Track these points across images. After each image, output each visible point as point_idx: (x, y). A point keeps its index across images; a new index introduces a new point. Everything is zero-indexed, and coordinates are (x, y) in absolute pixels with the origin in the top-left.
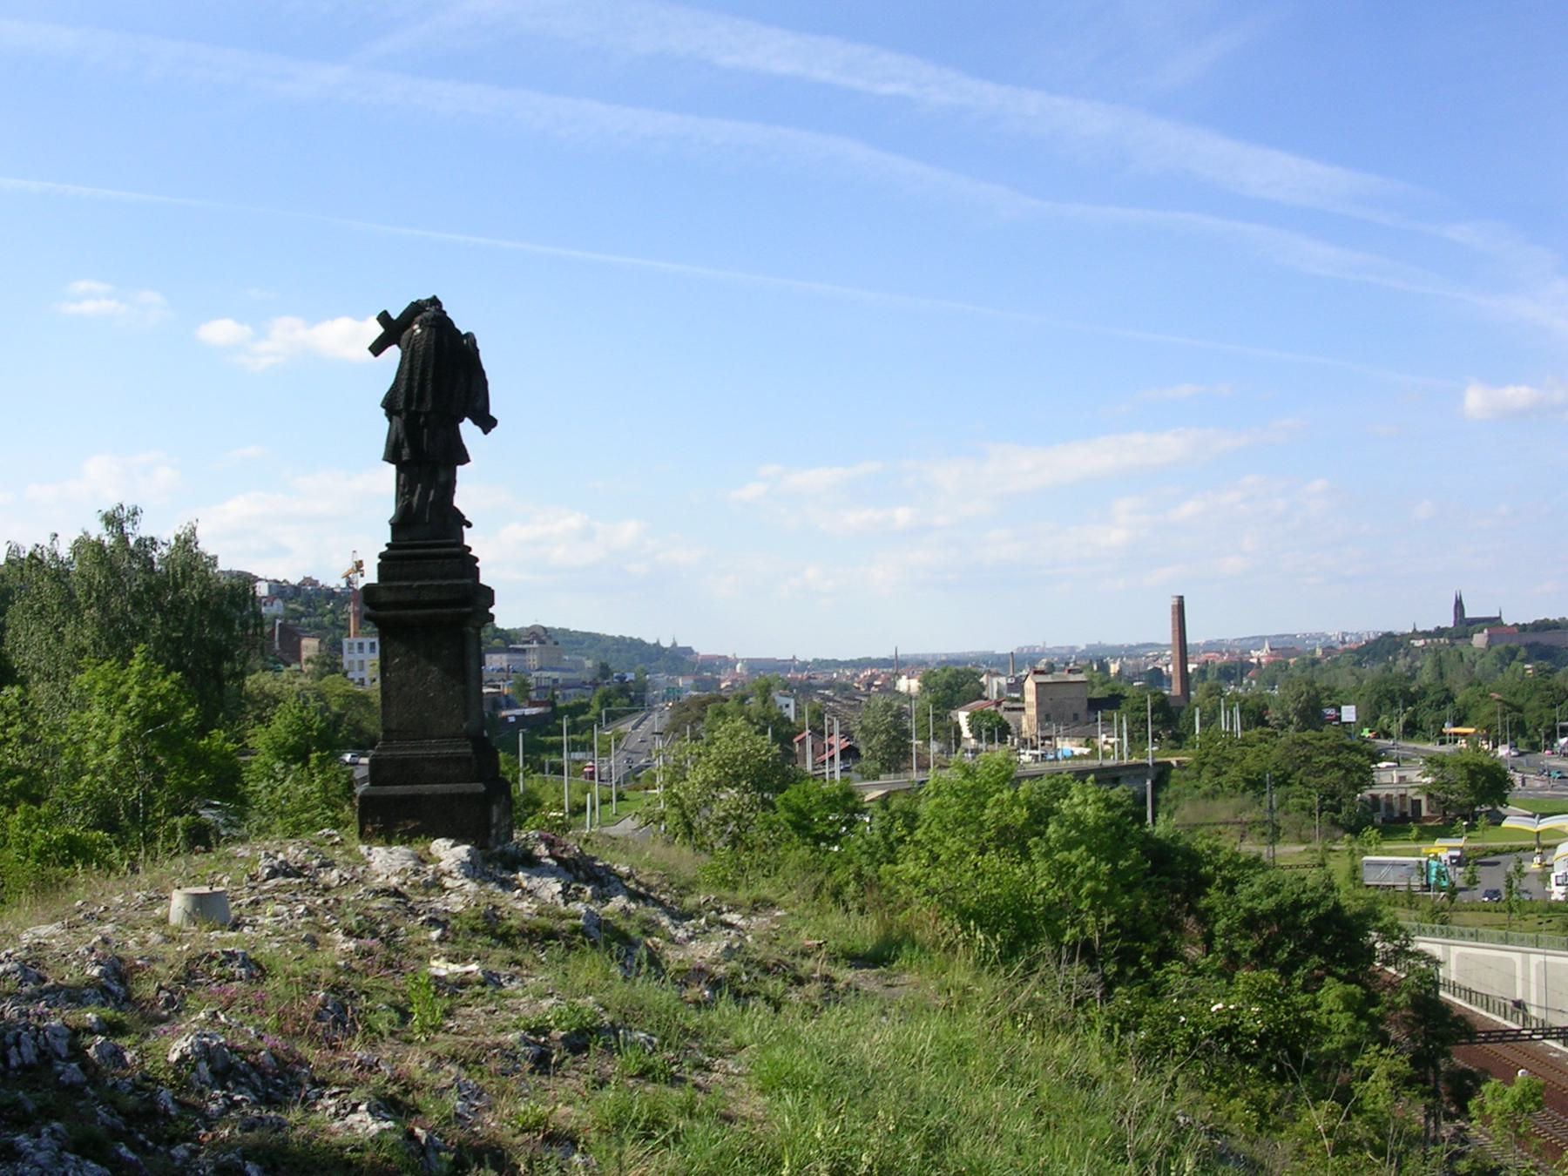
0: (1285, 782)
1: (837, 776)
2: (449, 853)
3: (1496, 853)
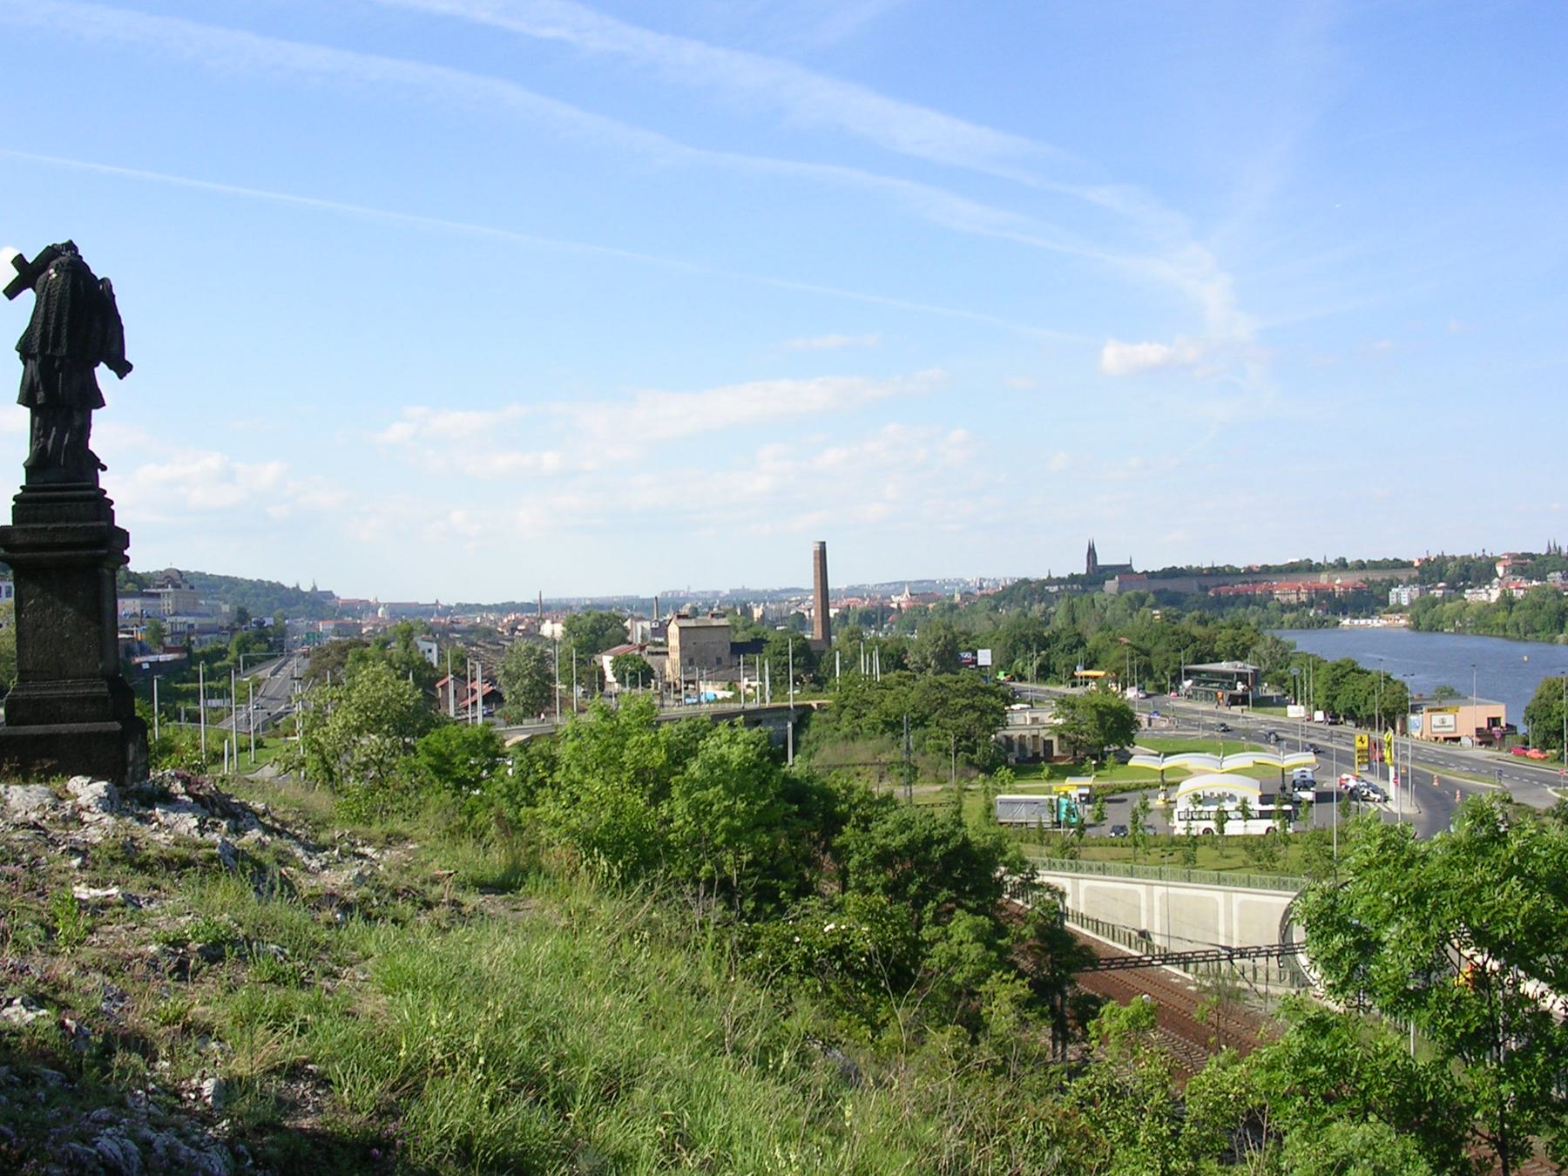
0: (922, 724)
1: (480, 721)
2: (86, 790)
3: (1123, 790)
